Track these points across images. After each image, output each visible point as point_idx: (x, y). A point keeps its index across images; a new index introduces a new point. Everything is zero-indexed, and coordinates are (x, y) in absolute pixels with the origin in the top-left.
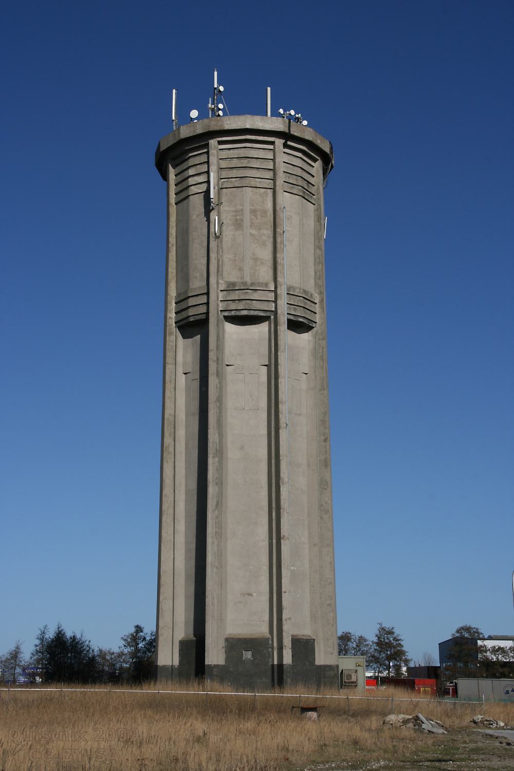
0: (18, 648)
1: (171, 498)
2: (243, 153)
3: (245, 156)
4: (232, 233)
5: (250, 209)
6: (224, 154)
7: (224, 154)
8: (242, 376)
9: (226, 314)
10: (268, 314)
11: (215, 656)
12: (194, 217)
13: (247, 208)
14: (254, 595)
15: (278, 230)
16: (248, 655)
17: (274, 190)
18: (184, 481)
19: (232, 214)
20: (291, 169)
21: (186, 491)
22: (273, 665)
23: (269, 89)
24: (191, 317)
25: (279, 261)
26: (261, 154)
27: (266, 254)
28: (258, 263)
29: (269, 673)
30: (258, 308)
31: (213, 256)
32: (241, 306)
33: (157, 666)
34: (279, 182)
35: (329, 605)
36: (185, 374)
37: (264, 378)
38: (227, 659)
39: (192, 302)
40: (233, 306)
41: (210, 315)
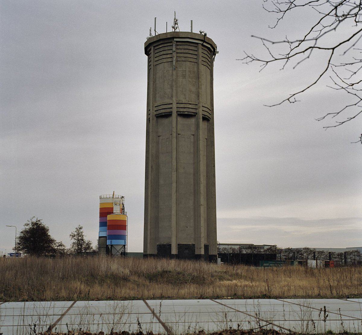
4: (181, 80)
9: (179, 113)
14: (189, 227)
20: (204, 59)
40: (182, 110)
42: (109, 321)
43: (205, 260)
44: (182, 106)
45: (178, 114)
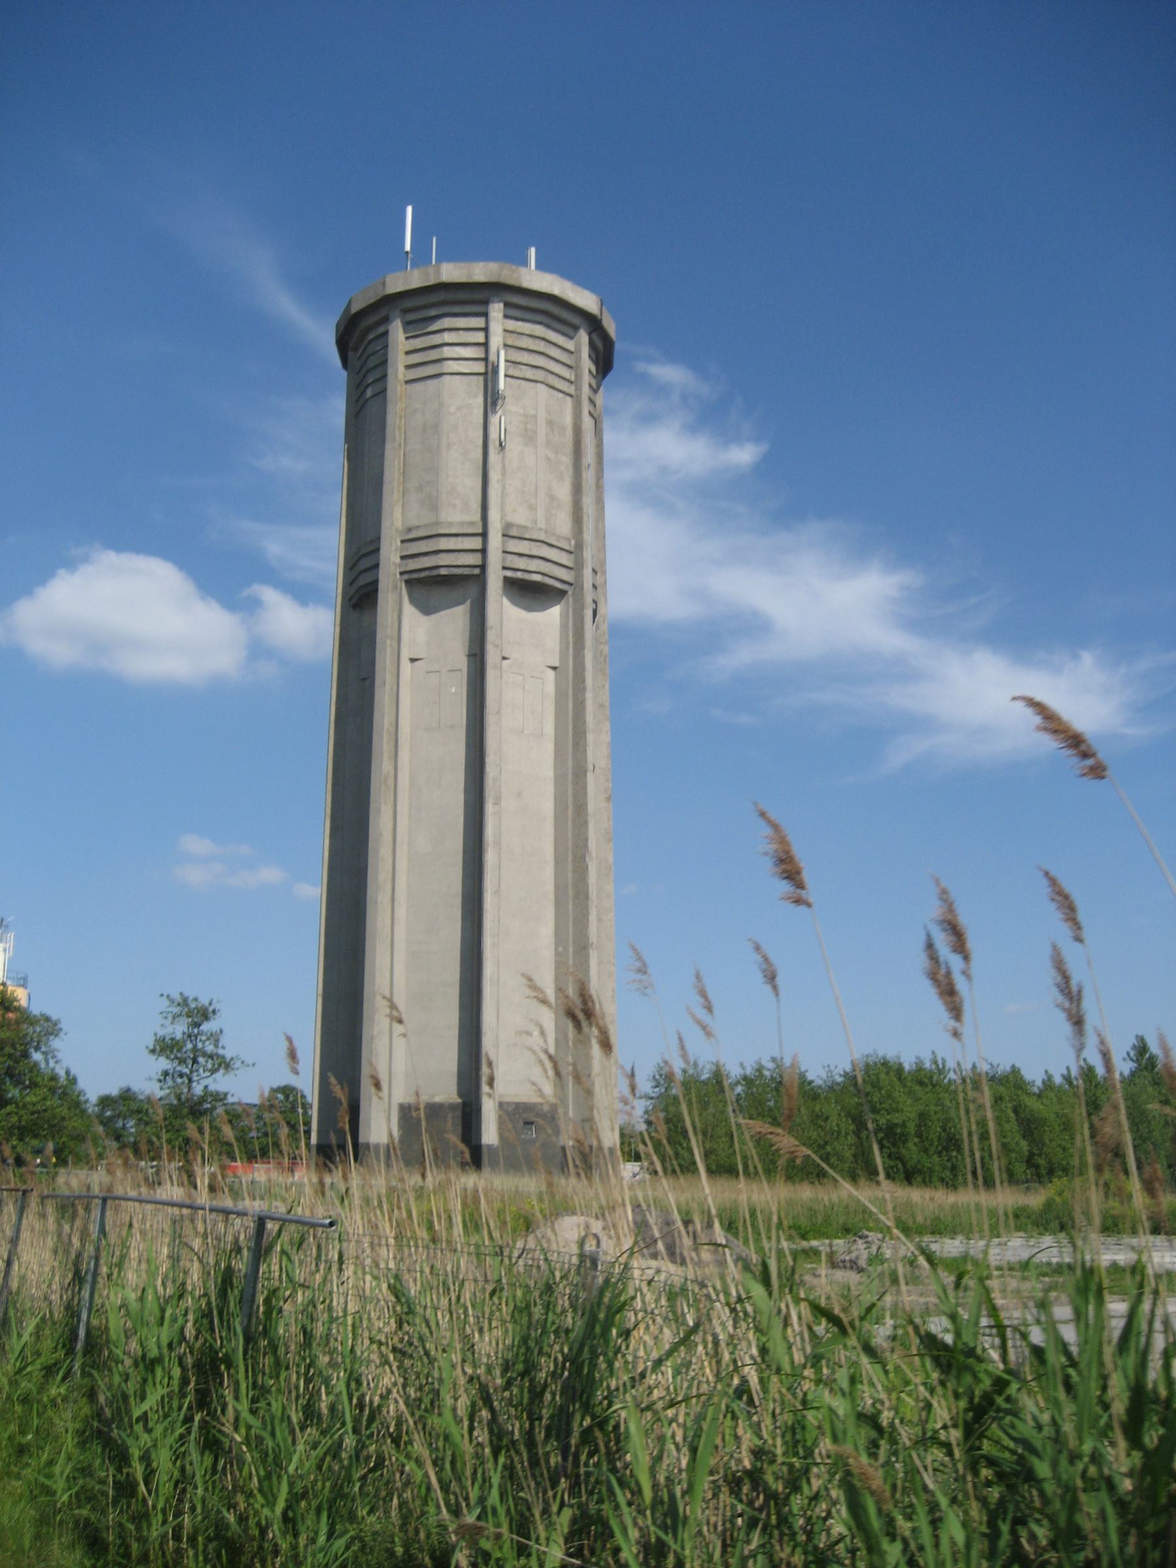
0: (1046, 1072)
1: (389, 866)
2: (539, 330)
6: (512, 325)
8: (521, 678)
9: (509, 574)
11: (490, 1135)
12: (452, 409)
13: (542, 416)
27: (564, 492)
31: (494, 476)
32: (533, 565)
37: (550, 688)
40: (521, 563)
44: (523, 547)
45: (506, 579)
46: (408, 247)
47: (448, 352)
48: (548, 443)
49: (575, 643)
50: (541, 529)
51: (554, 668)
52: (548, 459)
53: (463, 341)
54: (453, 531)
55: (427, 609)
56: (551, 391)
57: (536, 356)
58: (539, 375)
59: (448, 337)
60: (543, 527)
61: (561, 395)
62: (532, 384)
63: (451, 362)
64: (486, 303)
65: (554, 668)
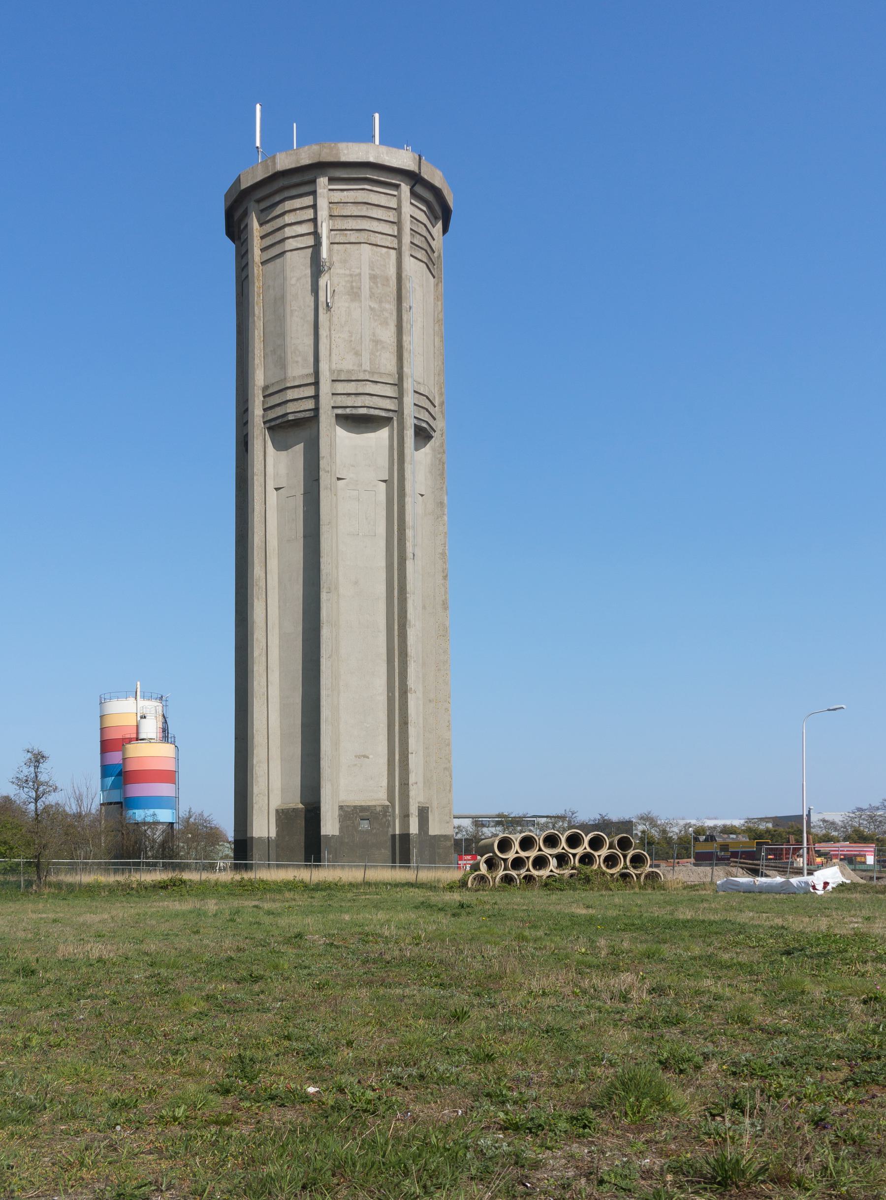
2: (361, 196)
3: (364, 201)
4: (347, 305)
5: (369, 274)
6: (337, 197)
7: (337, 197)
9: (340, 411)
10: (390, 414)
11: (330, 826)
12: (293, 281)
13: (366, 272)
14: (371, 756)
15: (405, 305)
16: (365, 825)
17: (399, 251)
18: (277, 622)
19: (346, 279)
21: (280, 634)
22: (394, 836)
23: (377, 116)
24: (290, 415)
25: (405, 344)
26: (383, 200)
27: (388, 335)
28: (379, 347)
29: (389, 844)
30: (383, 405)
31: (323, 332)
32: (359, 401)
33: (252, 838)
34: (407, 239)
35: (445, 769)
36: (277, 489)
37: (382, 497)
38: (341, 829)
39: (291, 394)
40: (350, 401)
41: (321, 411)
42: (195, 1039)
43: (183, 871)
44: (351, 388)
45: (337, 416)
46: (258, 144)
47: (288, 232)
48: (372, 295)
49: (399, 459)
50: (365, 371)
51: (385, 481)
52: (371, 309)
53: (299, 220)
54: (297, 384)
55: (280, 446)
56: (374, 247)
57: (359, 220)
58: (362, 237)
59: (288, 219)
60: (368, 369)
61: (385, 250)
62: (359, 245)
63: (291, 240)
64: (313, 182)
65: (385, 481)
